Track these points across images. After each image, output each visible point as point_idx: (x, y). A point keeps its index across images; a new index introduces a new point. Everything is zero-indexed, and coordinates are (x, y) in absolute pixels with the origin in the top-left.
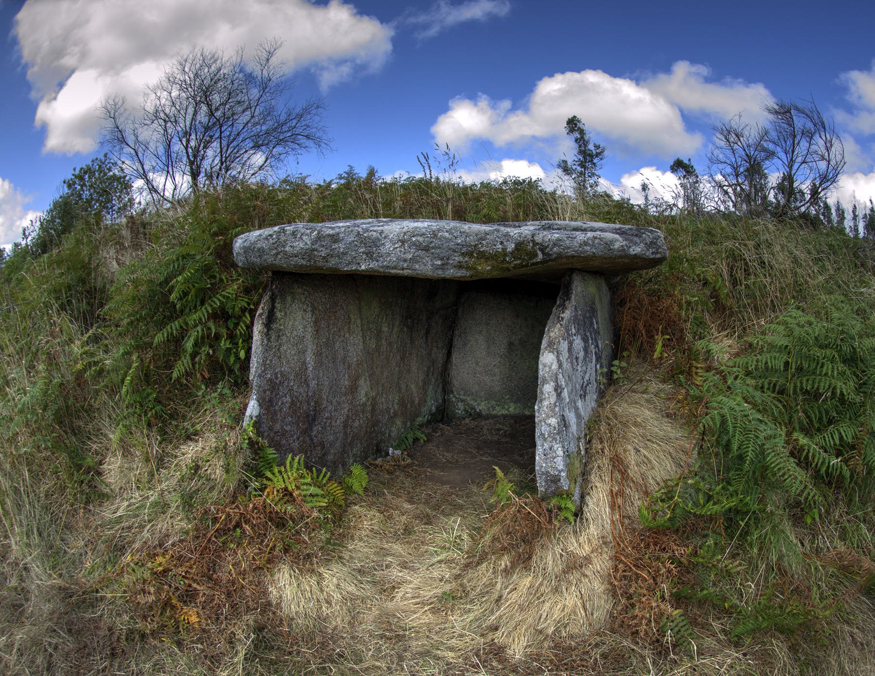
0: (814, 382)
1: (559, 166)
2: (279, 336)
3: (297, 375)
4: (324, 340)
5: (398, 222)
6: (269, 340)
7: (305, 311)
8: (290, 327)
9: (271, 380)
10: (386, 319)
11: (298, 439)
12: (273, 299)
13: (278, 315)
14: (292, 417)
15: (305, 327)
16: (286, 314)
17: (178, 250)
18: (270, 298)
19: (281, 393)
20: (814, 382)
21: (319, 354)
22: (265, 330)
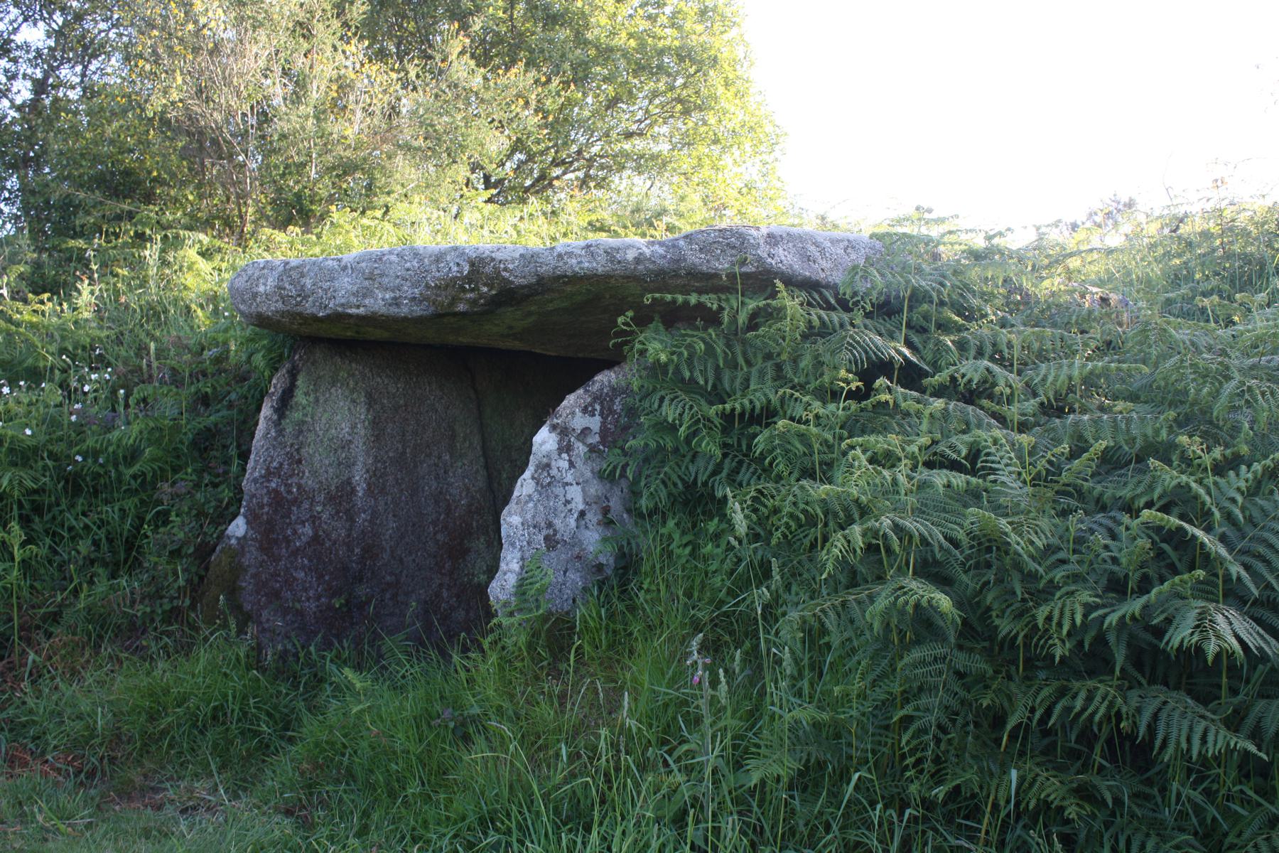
0: (1089, 699)
1: (1131, 200)
2: (301, 432)
3: (331, 499)
4: (391, 454)
5: (635, 243)
6: (280, 432)
7: (353, 401)
8: (324, 421)
9: (276, 491)
10: (1070, 316)
11: (318, 598)
12: (293, 374)
13: (300, 397)
14: (310, 561)
15: (353, 427)
16: (317, 400)
17: (188, 391)
18: (288, 372)
19: (293, 518)
20: (1089, 699)
21: (378, 474)
22: (275, 417)
